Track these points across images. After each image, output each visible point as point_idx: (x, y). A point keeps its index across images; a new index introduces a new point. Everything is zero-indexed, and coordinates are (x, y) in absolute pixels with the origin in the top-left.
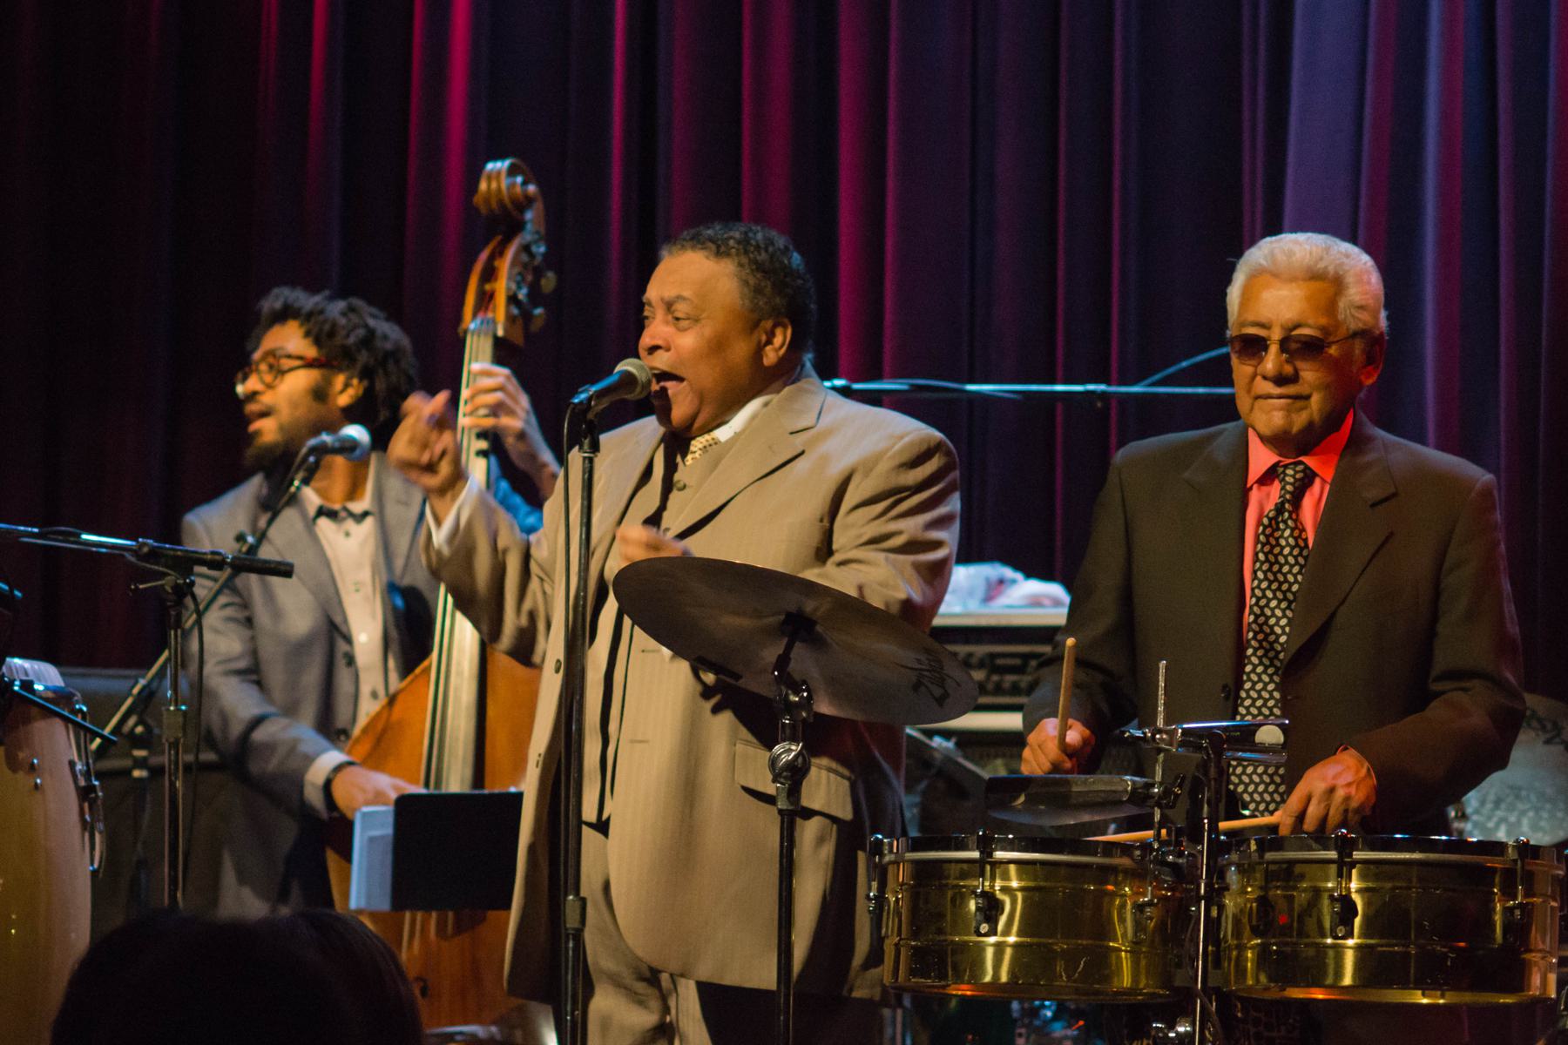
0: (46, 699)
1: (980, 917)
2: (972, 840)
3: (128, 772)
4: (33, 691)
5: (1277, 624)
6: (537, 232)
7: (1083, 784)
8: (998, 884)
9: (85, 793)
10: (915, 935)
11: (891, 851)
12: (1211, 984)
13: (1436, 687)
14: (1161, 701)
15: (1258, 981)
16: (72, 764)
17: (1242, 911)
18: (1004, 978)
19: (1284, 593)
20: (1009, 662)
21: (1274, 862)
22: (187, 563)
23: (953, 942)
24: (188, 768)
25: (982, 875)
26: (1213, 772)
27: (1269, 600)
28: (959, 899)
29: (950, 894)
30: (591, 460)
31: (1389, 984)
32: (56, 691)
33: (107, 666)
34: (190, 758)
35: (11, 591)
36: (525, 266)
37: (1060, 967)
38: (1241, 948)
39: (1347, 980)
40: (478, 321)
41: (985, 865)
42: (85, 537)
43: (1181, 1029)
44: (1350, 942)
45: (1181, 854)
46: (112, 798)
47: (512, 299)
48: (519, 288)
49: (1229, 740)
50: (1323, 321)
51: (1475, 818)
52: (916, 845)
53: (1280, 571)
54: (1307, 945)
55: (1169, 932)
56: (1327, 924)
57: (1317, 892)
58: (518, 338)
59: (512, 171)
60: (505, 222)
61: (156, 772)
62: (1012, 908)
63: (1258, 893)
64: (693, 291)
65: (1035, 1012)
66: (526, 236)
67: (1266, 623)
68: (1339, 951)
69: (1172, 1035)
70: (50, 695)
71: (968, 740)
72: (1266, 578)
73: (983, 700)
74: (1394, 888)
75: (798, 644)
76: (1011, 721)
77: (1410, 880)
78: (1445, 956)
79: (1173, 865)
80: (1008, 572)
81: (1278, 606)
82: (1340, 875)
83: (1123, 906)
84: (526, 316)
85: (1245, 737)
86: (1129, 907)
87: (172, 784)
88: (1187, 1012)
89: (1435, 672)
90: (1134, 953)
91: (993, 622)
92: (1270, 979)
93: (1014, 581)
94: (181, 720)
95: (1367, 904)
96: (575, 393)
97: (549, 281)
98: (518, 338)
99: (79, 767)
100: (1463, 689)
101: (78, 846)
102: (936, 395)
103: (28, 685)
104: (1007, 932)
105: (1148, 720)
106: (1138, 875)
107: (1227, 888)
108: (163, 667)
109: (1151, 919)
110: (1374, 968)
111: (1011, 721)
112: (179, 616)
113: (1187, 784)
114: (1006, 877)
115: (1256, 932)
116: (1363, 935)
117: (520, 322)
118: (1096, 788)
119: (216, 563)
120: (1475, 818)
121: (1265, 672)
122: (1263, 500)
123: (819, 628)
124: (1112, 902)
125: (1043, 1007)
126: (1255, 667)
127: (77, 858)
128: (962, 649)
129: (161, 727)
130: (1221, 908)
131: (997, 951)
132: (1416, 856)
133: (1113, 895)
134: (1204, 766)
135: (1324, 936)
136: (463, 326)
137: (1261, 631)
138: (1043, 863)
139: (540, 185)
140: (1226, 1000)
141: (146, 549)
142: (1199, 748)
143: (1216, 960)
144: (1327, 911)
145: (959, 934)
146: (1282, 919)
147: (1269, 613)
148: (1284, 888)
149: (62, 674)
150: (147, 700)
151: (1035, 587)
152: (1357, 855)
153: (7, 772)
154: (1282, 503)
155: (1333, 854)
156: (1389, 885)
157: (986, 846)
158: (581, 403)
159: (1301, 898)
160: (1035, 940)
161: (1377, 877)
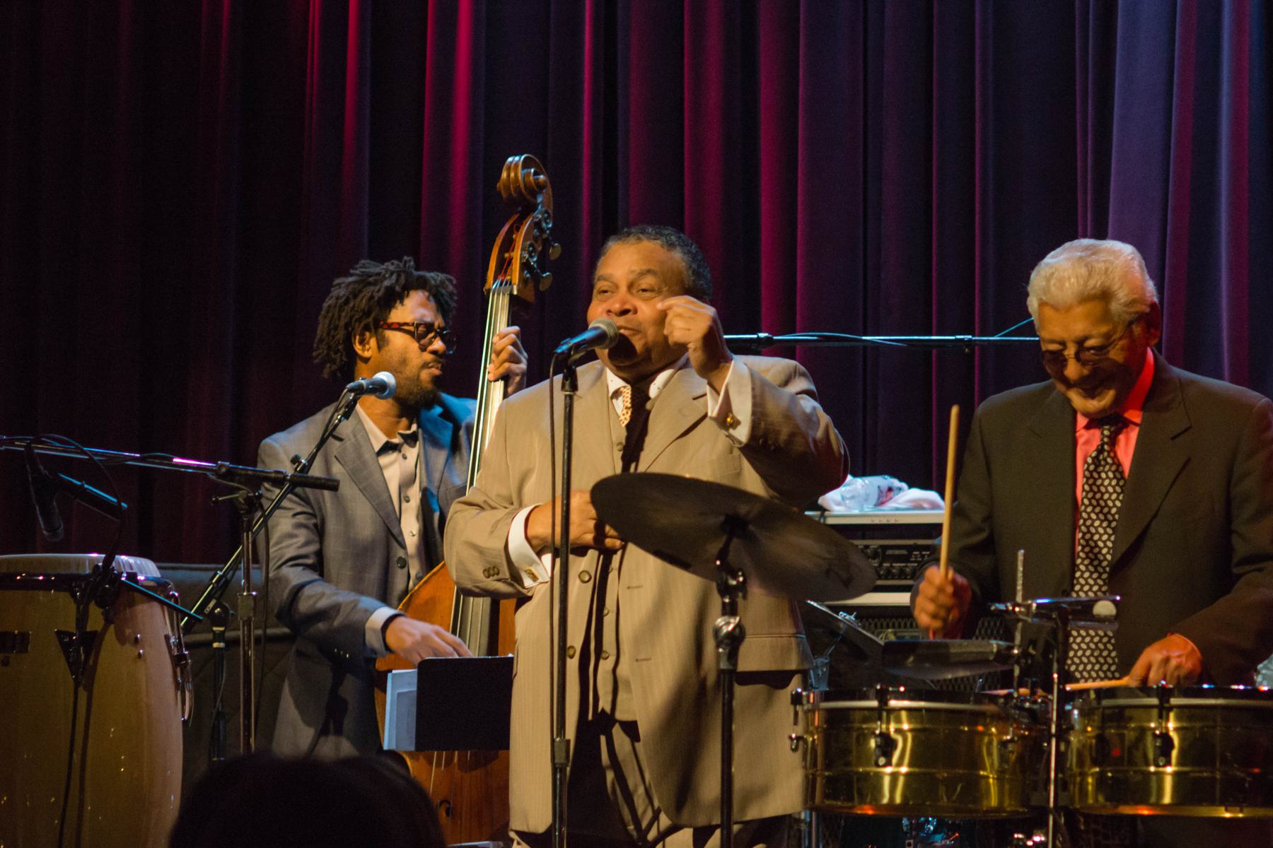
0: (147, 587)
1: (878, 752)
2: (872, 692)
3: (210, 643)
4: (137, 581)
5: (1100, 539)
6: (546, 212)
7: (960, 646)
8: (892, 727)
9: (177, 661)
10: (828, 766)
11: (808, 701)
12: (1061, 803)
13: (1236, 571)
14: (1020, 582)
15: (1096, 800)
16: (167, 638)
17: (1084, 746)
18: (898, 800)
19: (1105, 515)
20: (897, 552)
21: (1109, 708)
22: (257, 480)
23: (858, 773)
24: (258, 640)
25: (880, 719)
26: (1060, 636)
27: (1093, 521)
28: (863, 737)
29: (855, 734)
30: (571, 397)
31: (1199, 802)
32: (154, 580)
33: (190, 560)
34: (259, 632)
35: (119, 503)
36: (536, 239)
37: (942, 791)
38: (1083, 775)
39: (1167, 799)
40: (498, 282)
41: (883, 712)
42: (176, 460)
43: (1037, 839)
44: (1169, 769)
45: (1035, 702)
46: (198, 665)
47: (525, 266)
48: (531, 256)
49: (1074, 612)
50: (1104, 329)
51: (1264, 671)
52: (827, 697)
53: (1102, 498)
54: (1135, 772)
55: (1028, 762)
56: (1151, 755)
57: (1143, 731)
58: (530, 296)
59: (526, 164)
60: (523, 203)
61: (232, 643)
62: (904, 746)
63: (1097, 732)
64: (632, 275)
65: (920, 827)
66: (538, 215)
67: (1091, 539)
68: (1160, 776)
69: (1030, 843)
70: (151, 584)
71: (867, 614)
72: (1091, 504)
73: (879, 582)
74: (1202, 728)
75: (735, 540)
76: (902, 599)
77: (1215, 721)
78: (1244, 780)
79: (1029, 710)
80: (896, 483)
81: (1100, 526)
82: (1160, 717)
83: (990, 743)
84: (536, 279)
85: (1084, 610)
86: (996, 741)
87: (246, 653)
88: (1041, 825)
89: (1235, 560)
90: (1000, 780)
91: (884, 521)
92: (1107, 800)
93: (900, 489)
94: (252, 603)
95: (1182, 740)
96: (558, 345)
97: (555, 251)
98: (530, 296)
99: (172, 640)
100: (1260, 570)
101: (172, 702)
102: (841, 344)
103: (133, 576)
104: (899, 764)
105: (1012, 598)
106: (1002, 718)
107: (1072, 728)
108: (237, 561)
109: (1012, 752)
110: (1188, 789)
111: (902, 599)
112: (250, 521)
113: (1041, 644)
114: (899, 721)
115: (1095, 763)
116: (1179, 763)
117: (531, 285)
118: (969, 650)
119: (278, 480)
120: (1264, 671)
121: (1090, 577)
122: (1088, 441)
123: (751, 527)
124: (981, 740)
125: (928, 822)
126: (1083, 573)
127: (170, 711)
128: (860, 543)
129: (236, 610)
130: (1068, 743)
131: (893, 776)
132: (1220, 701)
133: (983, 734)
134: (1054, 632)
135: (1148, 765)
136: (487, 287)
137: (1088, 545)
138: (928, 710)
139: (549, 176)
140: (1071, 815)
141: (224, 470)
142: (1050, 618)
143: (1062, 785)
144: (1151, 747)
145: (861, 765)
146: (1115, 752)
147: (1093, 530)
148: (1118, 727)
149: (159, 568)
150: (224, 586)
151: (917, 493)
152: (1174, 701)
153: (118, 645)
154: (1102, 445)
155: (1155, 701)
156: (1198, 725)
157: (883, 697)
158: (563, 353)
159: (1130, 735)
160: (923, 770)
161: (1190, 718)
